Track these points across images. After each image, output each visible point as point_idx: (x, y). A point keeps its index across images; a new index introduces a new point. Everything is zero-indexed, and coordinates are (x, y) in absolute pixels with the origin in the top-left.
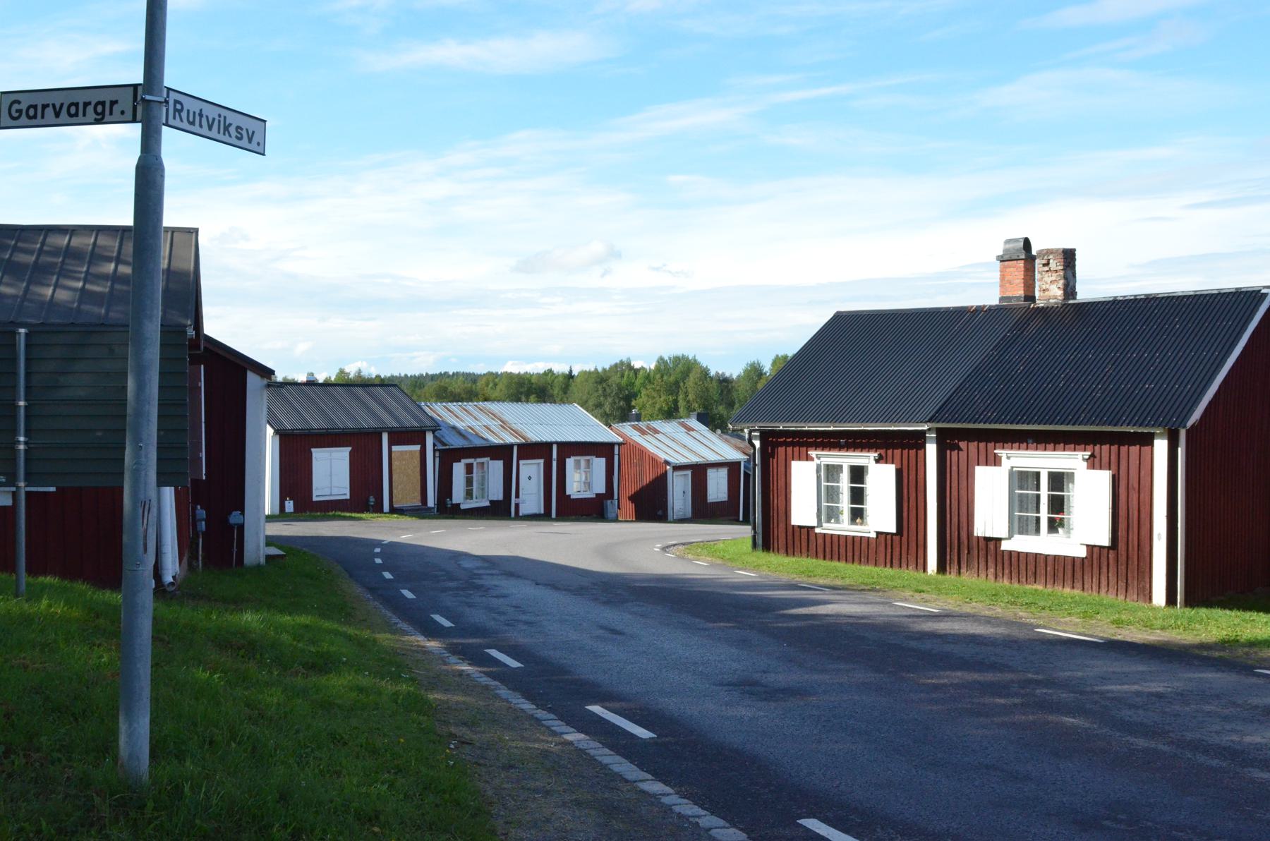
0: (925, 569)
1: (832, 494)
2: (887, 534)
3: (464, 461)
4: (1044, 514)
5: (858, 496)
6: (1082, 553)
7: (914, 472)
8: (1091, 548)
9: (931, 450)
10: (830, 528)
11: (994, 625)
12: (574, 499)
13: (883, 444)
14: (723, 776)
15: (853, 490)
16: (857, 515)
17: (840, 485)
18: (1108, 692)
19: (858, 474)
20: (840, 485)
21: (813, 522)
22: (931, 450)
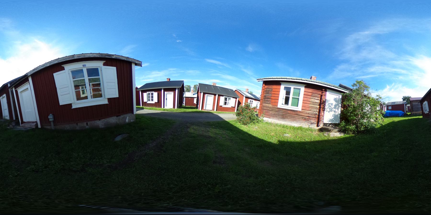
0: (162, 108)
1: (149, 97)
2: (153, 104)
3: (102, 101)
4: (151, 98)
5: (152, 97)
6: (154, 103)
7: (309, 96)
8: (155, 102)
9: (163, 91)
10: (149, 102)
11: (19, 81)
12: (41, 127)
13: (155, 90)
14: (187, 198)
15: (226, 100)
16: (152, 100)
17: (93, 93)
18: (193, 124)
19: (152, 94)
20: (93, 93)
21: (146, 101)
22: (163, 91)
